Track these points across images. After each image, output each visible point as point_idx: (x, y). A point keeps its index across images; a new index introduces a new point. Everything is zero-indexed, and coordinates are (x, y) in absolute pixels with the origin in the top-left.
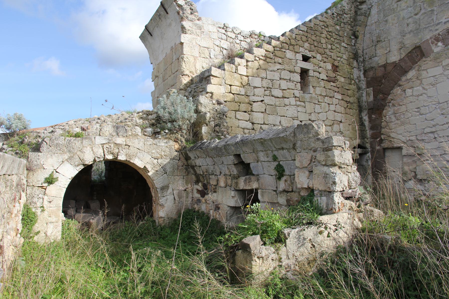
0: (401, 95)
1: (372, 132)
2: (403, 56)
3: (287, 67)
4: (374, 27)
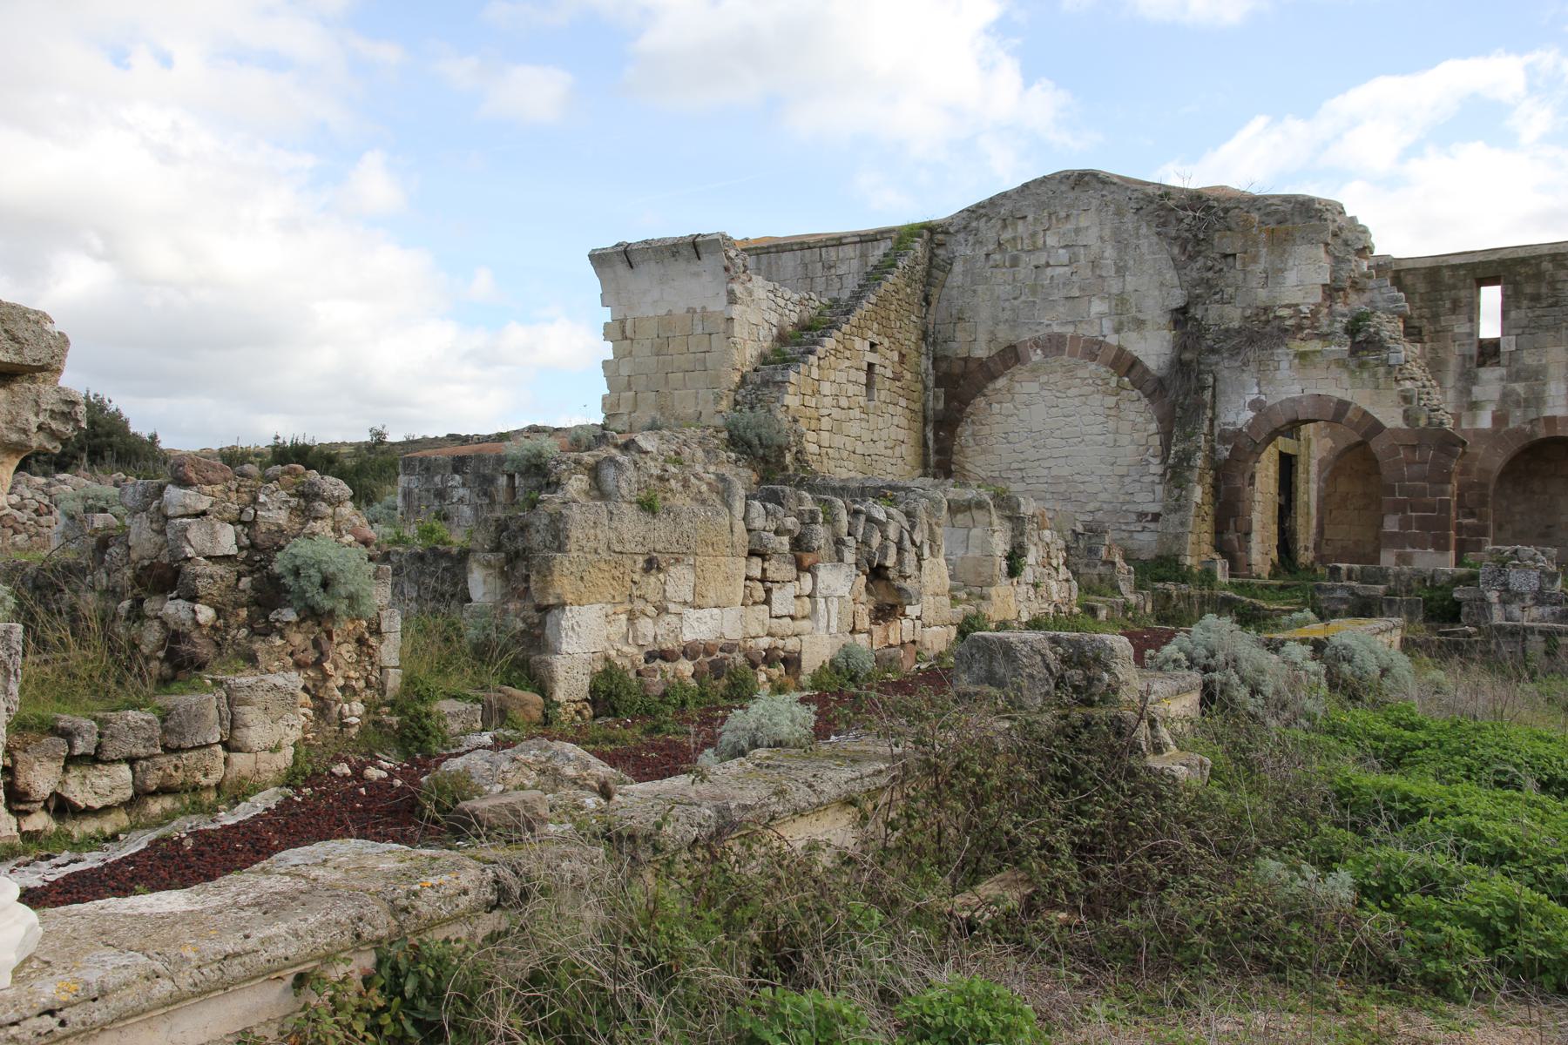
0: (985, 409)
1: (937, 458)
2: (992, 353)
3: (855, 365)
4: (955, 292)
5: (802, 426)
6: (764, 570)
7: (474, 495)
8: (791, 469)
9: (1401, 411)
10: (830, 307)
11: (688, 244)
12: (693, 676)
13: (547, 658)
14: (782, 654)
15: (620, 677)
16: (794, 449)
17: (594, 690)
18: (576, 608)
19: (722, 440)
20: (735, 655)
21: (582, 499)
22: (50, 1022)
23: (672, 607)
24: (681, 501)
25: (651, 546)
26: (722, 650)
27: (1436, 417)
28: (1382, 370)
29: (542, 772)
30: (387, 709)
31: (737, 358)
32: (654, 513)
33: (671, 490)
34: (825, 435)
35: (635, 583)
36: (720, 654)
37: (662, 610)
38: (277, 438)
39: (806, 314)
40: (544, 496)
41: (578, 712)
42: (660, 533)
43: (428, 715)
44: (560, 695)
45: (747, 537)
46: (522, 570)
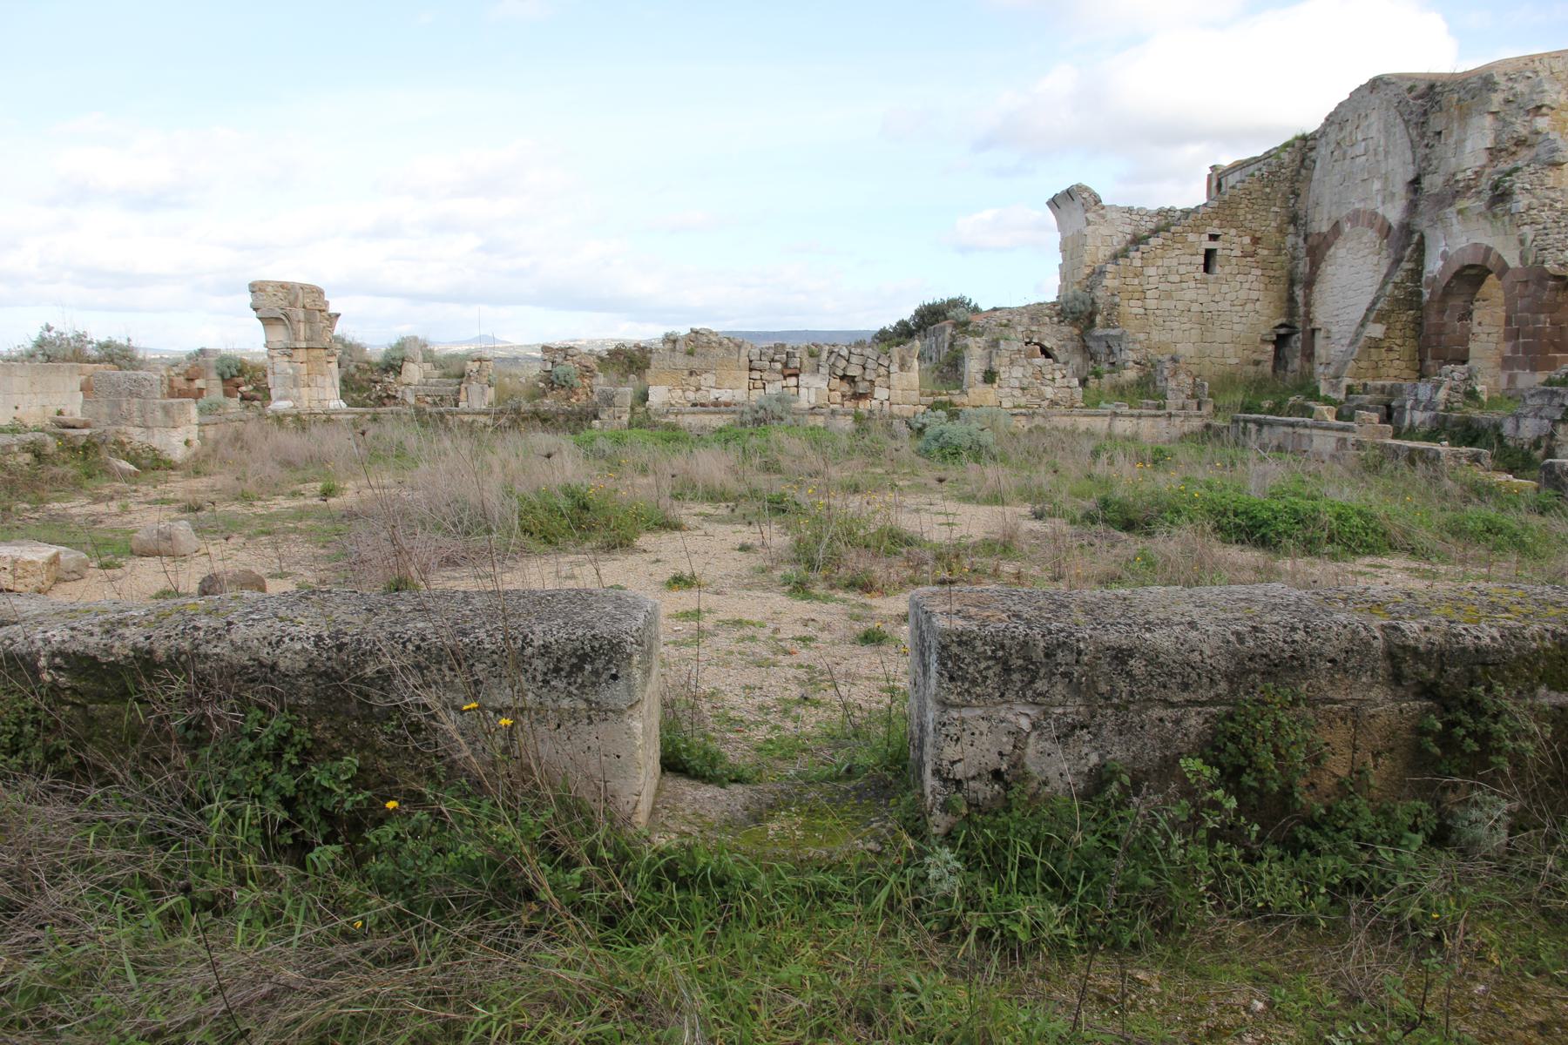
9: (1518, 252)
27: (1542, 255)
28: (1507, 218)
38: (49, 329)
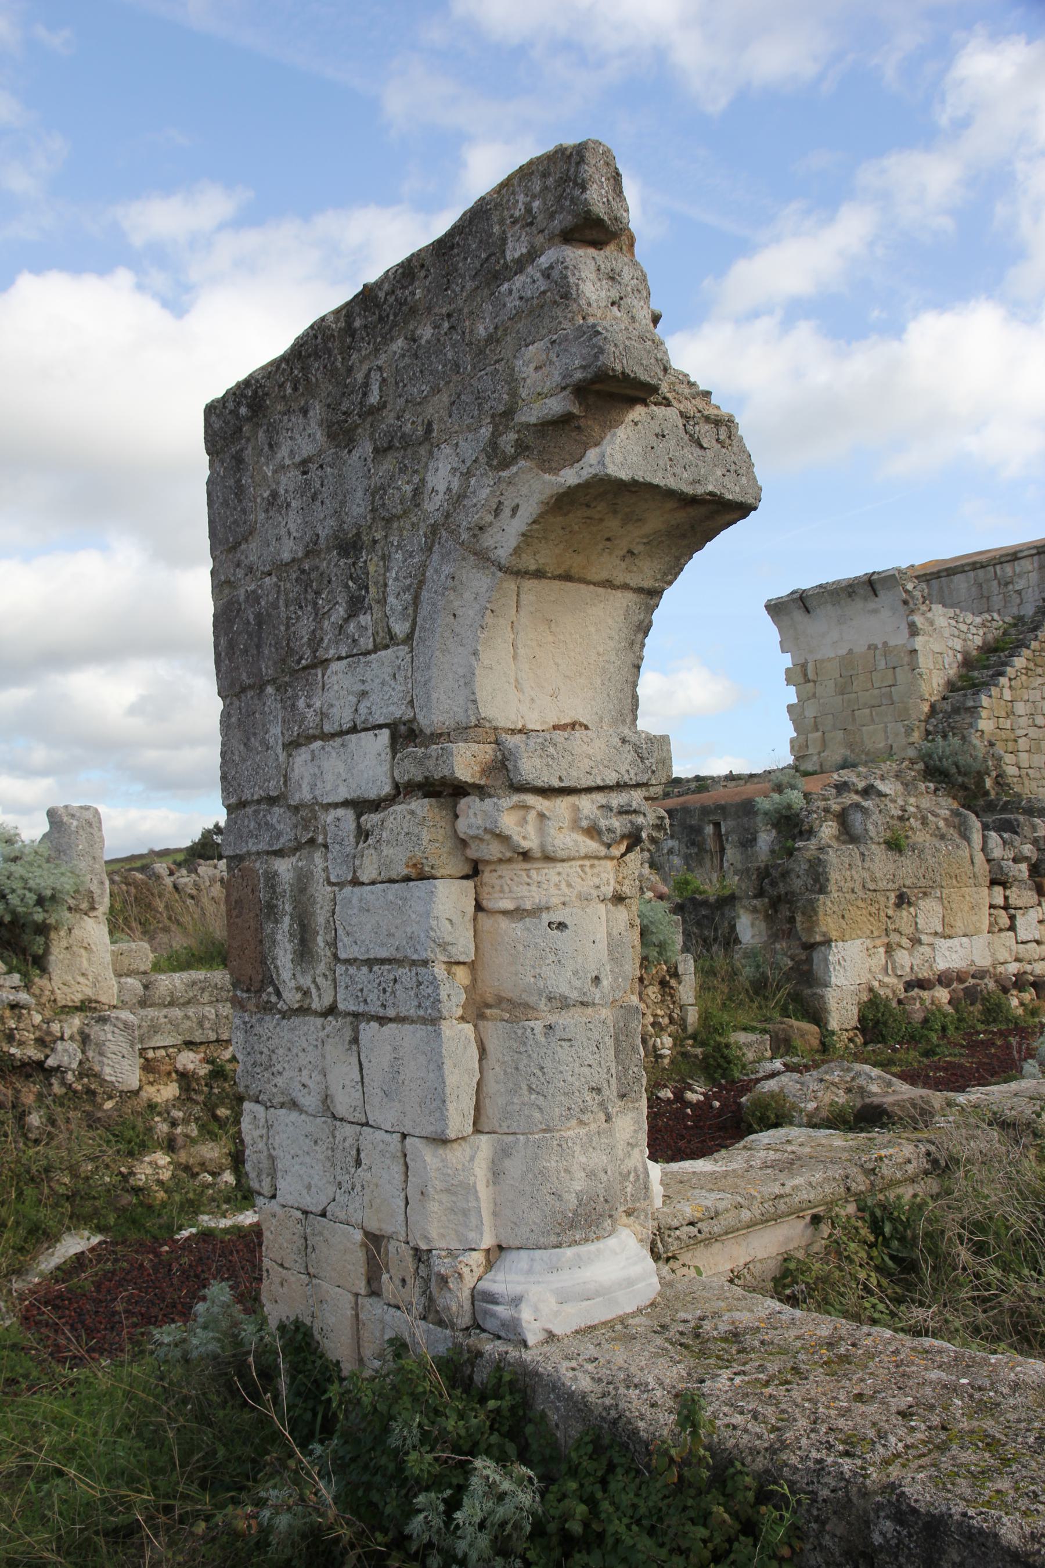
5: (999, 749)
6: (1006, 898)
7: (683, 846)
8: (993, 793)
10: (1015, 625)
11: (864, 583)
12: (949, 1003)
13: (819, 991)
14: (1031, 978)
15: (885, 1006)
16: (994, 774)
17: (862, 1019)
18: (840, 944)
19: (918, 772)
20: (986, 981)
21: (835, 844)
22: (693, 1230)
23: (925, 938)
24: (921, 837)
25: (901, 882)
26: (973, 977)
29: (849, 1090)
30: (690, 1042)
31: (925, 689)
32: (900, 851)
33: (912, 828)
34: (1024, 756)
35: (889, 918)
36: (972, 981)
37: (916, 941)
39: (990, 637)
40: (800, 844)
41: (851, 1040)
42: (908, 869)
43: (727, 1046)
44: (834, 1024)
45: (987, 867)
46: (785, 911)
